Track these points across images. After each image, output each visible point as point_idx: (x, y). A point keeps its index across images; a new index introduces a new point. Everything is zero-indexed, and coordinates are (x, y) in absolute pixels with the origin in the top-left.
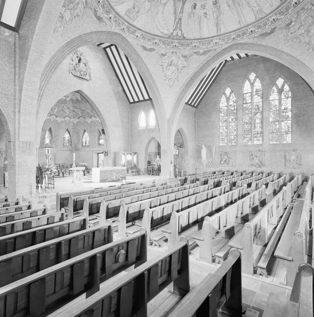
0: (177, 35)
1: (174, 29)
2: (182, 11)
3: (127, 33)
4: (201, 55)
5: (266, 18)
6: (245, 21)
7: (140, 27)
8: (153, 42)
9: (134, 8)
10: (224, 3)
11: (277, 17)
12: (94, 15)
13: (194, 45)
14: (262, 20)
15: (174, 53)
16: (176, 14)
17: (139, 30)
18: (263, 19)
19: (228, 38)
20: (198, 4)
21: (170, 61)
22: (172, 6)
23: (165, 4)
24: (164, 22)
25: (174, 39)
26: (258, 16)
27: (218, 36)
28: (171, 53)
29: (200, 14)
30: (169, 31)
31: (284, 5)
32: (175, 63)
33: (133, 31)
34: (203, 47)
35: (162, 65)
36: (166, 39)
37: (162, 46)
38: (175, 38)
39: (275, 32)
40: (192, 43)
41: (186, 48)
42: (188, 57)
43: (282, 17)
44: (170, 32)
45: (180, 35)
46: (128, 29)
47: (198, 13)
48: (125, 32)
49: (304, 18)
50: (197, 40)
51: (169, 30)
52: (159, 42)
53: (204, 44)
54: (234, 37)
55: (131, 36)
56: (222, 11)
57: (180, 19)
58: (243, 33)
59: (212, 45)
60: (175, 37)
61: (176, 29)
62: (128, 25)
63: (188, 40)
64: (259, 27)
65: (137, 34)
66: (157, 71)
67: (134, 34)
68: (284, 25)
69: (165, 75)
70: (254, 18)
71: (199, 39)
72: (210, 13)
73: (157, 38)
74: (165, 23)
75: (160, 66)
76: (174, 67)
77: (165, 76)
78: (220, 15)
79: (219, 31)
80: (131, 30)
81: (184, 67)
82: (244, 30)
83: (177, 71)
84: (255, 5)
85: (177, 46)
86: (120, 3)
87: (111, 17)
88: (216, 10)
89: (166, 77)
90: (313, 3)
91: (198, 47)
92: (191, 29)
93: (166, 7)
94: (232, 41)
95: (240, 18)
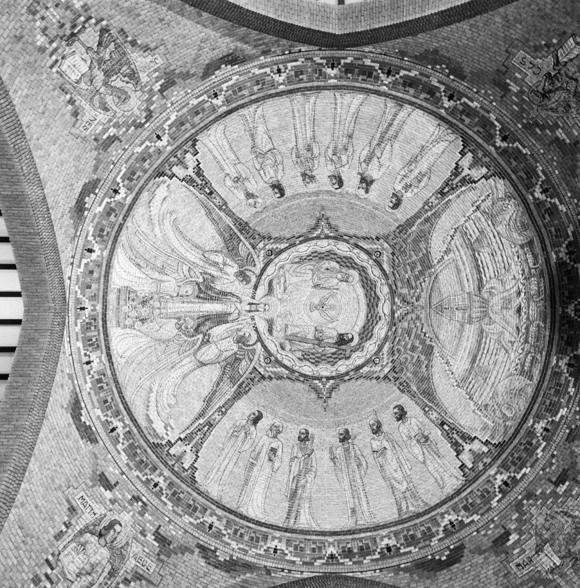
0: (179, 458)
1: (182, 436)
2: (223, 410)
3: (79, 325)
4: (218, 565)
5: (429, 516)
6: (371, 513)
7: (115, 352)
8: (109, 419)
9: (144, 303)
10: (324, 448)
11: (460, 518)
12: (85, 185)
13: (209, 519)
14: (417, 521)
15: (140, 504)
16: (208, 405)
17: (109, 356)
18: (421, 519)
19: (314, 550)
20: (267, 417)
21: (110, 517)
22: (211, 381)
23: (203, 364)
24: (172, 401)
25: (166, 464)
26: (407, 507)
27: (286, 530)
28: (130, 497)
29: (260, 445)
30: (167, 430)
31: (475, 485)
32: (121, 540)
33: (94, 339)
34: (234, 544)
35: (72, 510)
36: (144, 444)
37: (122, 452)
38: (170, 463)
39: (462, 559)
40: (206, 509)
41: (181, 513)
42: (171, 547)
43: (476, 517)
44: (167, 434)
45: (186, 466)
46: (90, 324)
47: (257, 440)
48: (77, 317)
49: (541, 520)
50: (226, 511)
51: (169, 428)
52: (122, 436)
53: (239, 534)
54: (335, 552)
55: (80, 344)
56: (314, 464)
57: (210, 425)
58: (361, 549)
59: (262, 552)
60: (172, 461)
61: (187, 443)
62: (100, 317)
63: (200, 493)
64: (411, 541)
65: (93, 357)
66: (41, 512)
67: (90, 349)
68: (487, 543)
69: (50, 558)
70: (395, 510)
71: (231, 511)
72: (284, 455)
73: (128, 421)
74: (173, 403)
75: (66, 504)
76: (105, 553)
77: (47, 561)
78: (306, 473)
79: (293, 515)
80: (92, 333)
81: (138, 577)
82: (366, 538)
83: (105, 574)
84: (399, 475)
85: (162, 489)
86: (133, 258)
87: (94, 251)
88: (300, 455)
89: (49, 571)
90: (554, 479)
91: (218, 535)
92: (222, 469)
93: (197, 372)
94: (327, 564)
95: (356, 501)
